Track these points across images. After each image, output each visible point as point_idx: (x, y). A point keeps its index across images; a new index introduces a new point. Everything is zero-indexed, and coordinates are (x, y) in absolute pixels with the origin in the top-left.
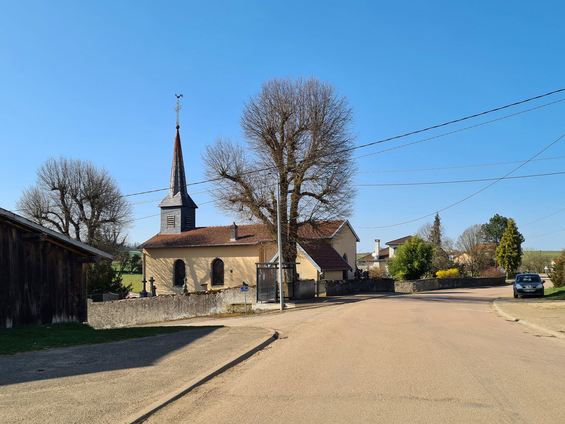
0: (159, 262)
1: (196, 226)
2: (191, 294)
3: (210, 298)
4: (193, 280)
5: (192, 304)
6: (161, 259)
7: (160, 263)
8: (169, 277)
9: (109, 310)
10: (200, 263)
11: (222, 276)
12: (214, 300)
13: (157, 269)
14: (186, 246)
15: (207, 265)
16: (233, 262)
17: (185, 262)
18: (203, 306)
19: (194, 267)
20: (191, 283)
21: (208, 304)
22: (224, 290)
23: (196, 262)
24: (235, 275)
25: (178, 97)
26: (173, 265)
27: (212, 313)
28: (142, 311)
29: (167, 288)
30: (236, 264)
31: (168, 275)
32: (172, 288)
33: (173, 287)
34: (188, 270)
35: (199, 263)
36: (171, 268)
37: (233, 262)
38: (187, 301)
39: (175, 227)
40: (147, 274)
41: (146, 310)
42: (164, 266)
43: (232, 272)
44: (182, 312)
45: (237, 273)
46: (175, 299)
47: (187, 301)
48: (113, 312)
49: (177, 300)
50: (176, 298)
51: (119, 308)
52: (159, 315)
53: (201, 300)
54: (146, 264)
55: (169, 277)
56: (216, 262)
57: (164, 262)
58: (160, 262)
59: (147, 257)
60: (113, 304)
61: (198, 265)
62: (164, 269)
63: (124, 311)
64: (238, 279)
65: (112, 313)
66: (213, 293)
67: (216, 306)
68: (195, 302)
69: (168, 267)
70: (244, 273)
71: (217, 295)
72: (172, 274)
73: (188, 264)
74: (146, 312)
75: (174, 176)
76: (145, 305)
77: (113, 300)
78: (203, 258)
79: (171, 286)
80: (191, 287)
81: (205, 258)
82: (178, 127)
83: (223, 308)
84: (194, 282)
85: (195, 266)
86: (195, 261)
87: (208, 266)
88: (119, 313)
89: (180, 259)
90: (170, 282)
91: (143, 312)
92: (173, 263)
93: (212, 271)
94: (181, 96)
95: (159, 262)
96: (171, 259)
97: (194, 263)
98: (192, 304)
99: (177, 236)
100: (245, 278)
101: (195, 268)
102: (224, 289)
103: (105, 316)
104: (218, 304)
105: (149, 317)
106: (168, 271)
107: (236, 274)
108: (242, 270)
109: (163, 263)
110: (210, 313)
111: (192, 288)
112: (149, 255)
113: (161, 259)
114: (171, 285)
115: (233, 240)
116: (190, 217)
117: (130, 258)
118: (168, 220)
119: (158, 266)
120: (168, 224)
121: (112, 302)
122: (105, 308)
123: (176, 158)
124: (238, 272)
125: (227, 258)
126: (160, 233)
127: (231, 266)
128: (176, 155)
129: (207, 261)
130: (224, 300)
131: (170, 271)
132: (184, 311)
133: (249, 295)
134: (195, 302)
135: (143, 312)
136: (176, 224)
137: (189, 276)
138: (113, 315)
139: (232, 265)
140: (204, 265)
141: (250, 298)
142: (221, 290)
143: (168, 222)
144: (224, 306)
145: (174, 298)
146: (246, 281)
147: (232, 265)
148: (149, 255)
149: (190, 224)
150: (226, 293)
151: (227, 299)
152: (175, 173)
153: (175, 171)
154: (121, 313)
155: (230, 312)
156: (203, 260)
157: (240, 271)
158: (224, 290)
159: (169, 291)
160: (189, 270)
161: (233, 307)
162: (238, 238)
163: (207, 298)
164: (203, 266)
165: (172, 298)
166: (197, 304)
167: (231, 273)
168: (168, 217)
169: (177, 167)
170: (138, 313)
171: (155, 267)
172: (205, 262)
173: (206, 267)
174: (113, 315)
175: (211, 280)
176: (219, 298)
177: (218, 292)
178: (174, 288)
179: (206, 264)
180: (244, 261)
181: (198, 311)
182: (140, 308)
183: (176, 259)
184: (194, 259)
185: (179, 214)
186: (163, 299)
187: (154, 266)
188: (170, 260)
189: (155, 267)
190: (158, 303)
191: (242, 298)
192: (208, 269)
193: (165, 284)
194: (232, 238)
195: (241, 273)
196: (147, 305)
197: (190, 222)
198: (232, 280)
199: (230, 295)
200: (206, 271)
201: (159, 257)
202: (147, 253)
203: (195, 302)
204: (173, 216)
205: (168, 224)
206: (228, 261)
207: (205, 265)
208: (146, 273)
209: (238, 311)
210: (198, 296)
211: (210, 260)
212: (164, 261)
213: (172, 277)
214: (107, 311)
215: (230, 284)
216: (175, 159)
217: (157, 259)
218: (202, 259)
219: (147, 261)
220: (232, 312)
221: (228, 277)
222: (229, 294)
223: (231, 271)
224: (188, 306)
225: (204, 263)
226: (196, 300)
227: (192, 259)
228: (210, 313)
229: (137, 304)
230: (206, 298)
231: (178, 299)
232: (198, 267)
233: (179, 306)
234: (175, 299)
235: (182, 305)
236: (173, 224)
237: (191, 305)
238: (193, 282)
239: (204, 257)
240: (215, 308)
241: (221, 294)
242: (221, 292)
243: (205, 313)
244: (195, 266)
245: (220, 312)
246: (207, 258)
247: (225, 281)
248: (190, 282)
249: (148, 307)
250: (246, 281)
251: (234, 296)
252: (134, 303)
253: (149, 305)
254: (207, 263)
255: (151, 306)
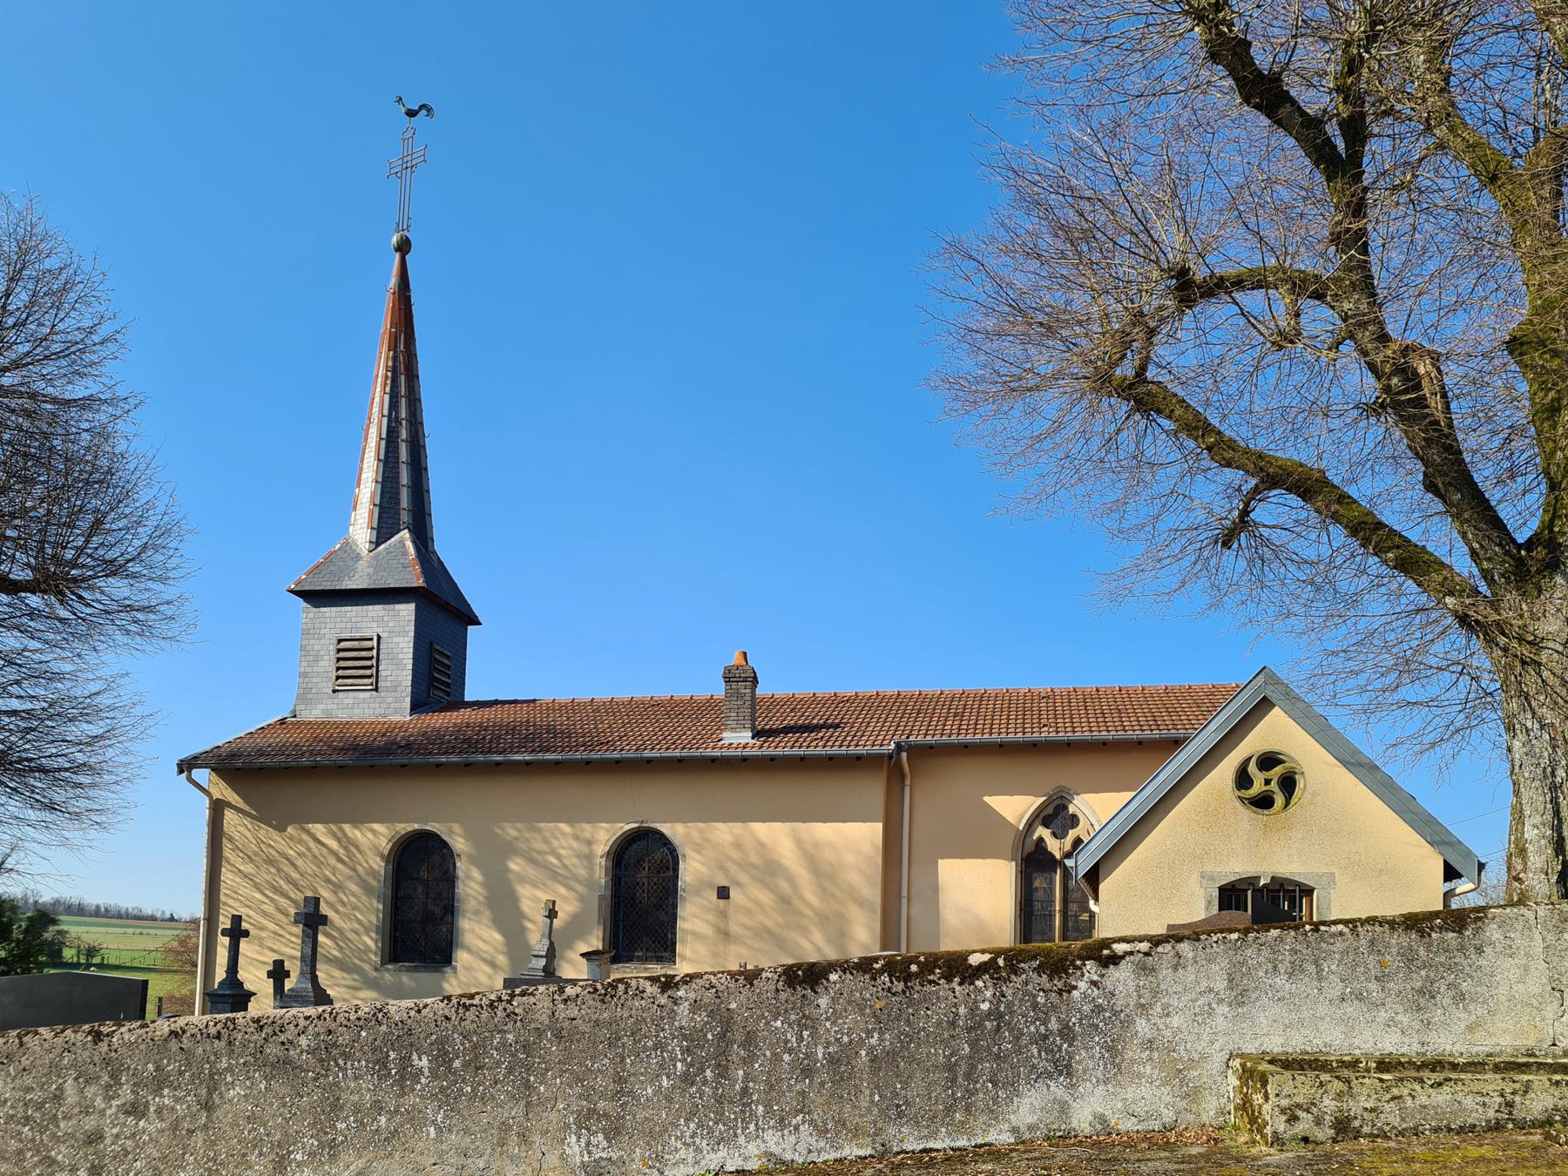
0: (301, 841)
1: (468, 698)
2: (833, 977)
3: (1010, 1005)
4: (498, 937)
5: (850, 1051)
6: (318, 829)
7: (309, 849)
8: (359, 922)
9: (58, 1097)
10: (545, 848)
11: (663, 916)
12: (1054, 1025)
13: (289, 880)
14: (481, 758)
15: (585, 863)
16: (738, 846)
17: (459, 843)
18: (951, 1068)
19: (508, 870)
20: (492, 951)
21: (998, 1057)
22: (1144, 946)
23: (522, 846)
24: (749, 912)
25: (411, 114)
26: (382, 856)
27: (1031, 1128)
28: (378, 1107)
29: (346, 975)
30: (754, 859)
31: (355, 908)
32: (375, 974)
33: (376, 969)
34: (471, 884)
35: (538, 852)
36: (373, 873)
37: (738, 846)
38: (802, 1027)
39: (376, 690)
40: (230, 902)
41: (412, 1100)
42: (333, 861)
43: (728, 897)
44: (747, 1116)
45: (756, 902)
46: (683, 1009)
47: (802, 1027)
48: (102, 1113)
49: (700, 1018)
50: (696, 1006)
51: (160, 1082)
52: (537, 1138)
53: (930, 1018)
54: (227, 852)
55: (359, 922)
56: (630, 845)
57: (334, 844)
58: (312, 844)
59: (229, 815)
60: (103, 1047)
61: (532, 861)
62: (328, 881)
63: (208, 1107)
64: (764, 933)
65: (90, 1123)
66: (1039, 970)
67: (1064, 1068)
68: (874, 1041)
69: (354, 870)
70: (796, 902)
71: (1082, 985)
72: (375, 902)
73: (473, 852)
74: (415, 1119)
75: (382, 457)
76: (405, 1062)
77: (102, 1021)
78: (562, 825)
79: (366, 967)
80: (487, 969)
81: (577, 825)
82: (404, 247)
83: (1131, 1093)
84: (507, 944)
85: (515, 865)
86: (517, 839)
87: (591, 868)
88: (151, 1126)
89: (431, 827)
90: (365, 944)
91: (383, 1120)
92: (385, 845)
93: (609, 893)
94: (424, 112)
95: (301, 841)
96: (376, 826)
97: (510, 849)
98: (850, 1051)
99: (401, 726)
100: (805, 931)
101: (512, 877)
102: (1141, 939)
103: (20, 1152)
104: (1087, 1058)
105: (441, 1154)
106: (353, 887)
107: (752, 906)
108: (784, 885)
109: (324, 851)
110: (1015, 1130)
111: (490, 977)
112: (247, 808)
113: (319, 826)
114: (369, 962)
115: (745, 737)
116: (448, 657)
117: (21, 920)
118: (342, 654)
119: (299, 863)
120: (341, 673)
121: (98, 1037)
122: (28, 1080)
123: (393, 381)
124: (764, 897)
125: (701, 824)
126: (295, 716)
127: (723, 868)
128: (390, 364)
129: (589, 843)
130: (1142, 1027)
131: (367, 888)
132: (769, 1111)
133: (1373, 986)
134: (874, 1041)
135: (383, 1120)
136: (382, 674)
137: (476, 912)
138: (101, 1138)
139: (734, 861)
140: (567, 862)
141: (1383, 1015)
142: (1120, 948)
143: (342, 664)
144: (1139, 1076)
145: (675, 1002)
146: (812, 943)
147: (734, 861)
148: (247, 808)
149: (448, 685)
150: (1165, 972)
151: (1175, 1021)
152: (383, 443)
153: (384, 436)
154: (175, 1127)
155: (1305, 1125)
156: (563, 834)
157: (771, 891)
158: (1144, 946)
159: (356, 989)
160: (481, 884)
161: (1338, 1086)
162: (757, 734)
163: (985, 1006)
164: (565, 866)
165: (663, 1000)
166: (892, 1055)
167: (722, 902)
168: (340, 641)
169: (398, 421)
170: (341, 1126)
171: (279, 870)
172: (575, 845)
173: (583, 872)
174: (95, 1138)
175: (601, 934)
176: (1099, 1009)
177: (1084, 959)
178: (387, 976)
179: (578, 856)
180: (799, 842)
181: (898, 1112)
182: (360, 1088)
183: (405, 828)
184: (513, 833)
185: (402, 634)
186: (573, 1011)
187: (270, 861)
188: (370, 836)
189: (279, 870)
190: (527, 1048)
191: (1306, 1014)
192: (590, 883)
193: (336, 953)
194: (733, 730)
195: (785, 902)
196: (425, 1062)
197: (449, 676)
198: (725, 935)
199: (1204, 984)
200: (579, 888)
201: (302, 819)
202: (232, 796)
203: (869, 1033)
204: (367, 635)
205: (341, 673)
206: (707, 840)
207: (575, 861)
208: (223, 898)
209: (1391, 1116)
210: (899, 986)
211: (604, 836)
212: (339, 840)
213: (374, 920)
214: (39, 1106)
215: (715, 955)
216: (389, 382)
217: (290, 829)
218: (559, 829)
219: (231, 839)
220: (1327, 1133)
221: (707, 922)
222: (1189, 975)
223: (723, 893)
224: (808, 1072)
225: (571, 848)
226: (881, 1021)
227: (498, 831)
228: (1015, 1130)
229: (328, 1052)
230: (973, 1010)
231: (711, 1014)
232: (531, 871)
233: (723, 1072)
234: (683, 1009)
235: (748, 1061)
236: (369, 677)
237: (833, 1061)
238: (501, 948)
239: (570, 822)
240: (1057, 1089)
241: (1121, 977)
242: (1115, 960)
243: (962, 1128)
244: (513, 866)
245: (1102, 1119)
246: (587, 827)
247: (683, 941)
248: (481, 945)
249: (434, 1075)
250: (812, 943)
251: (1240, 996)
252: (303, 1041)
253: (442, 1058)
254: (585, 849)
255: (466, 1065)
